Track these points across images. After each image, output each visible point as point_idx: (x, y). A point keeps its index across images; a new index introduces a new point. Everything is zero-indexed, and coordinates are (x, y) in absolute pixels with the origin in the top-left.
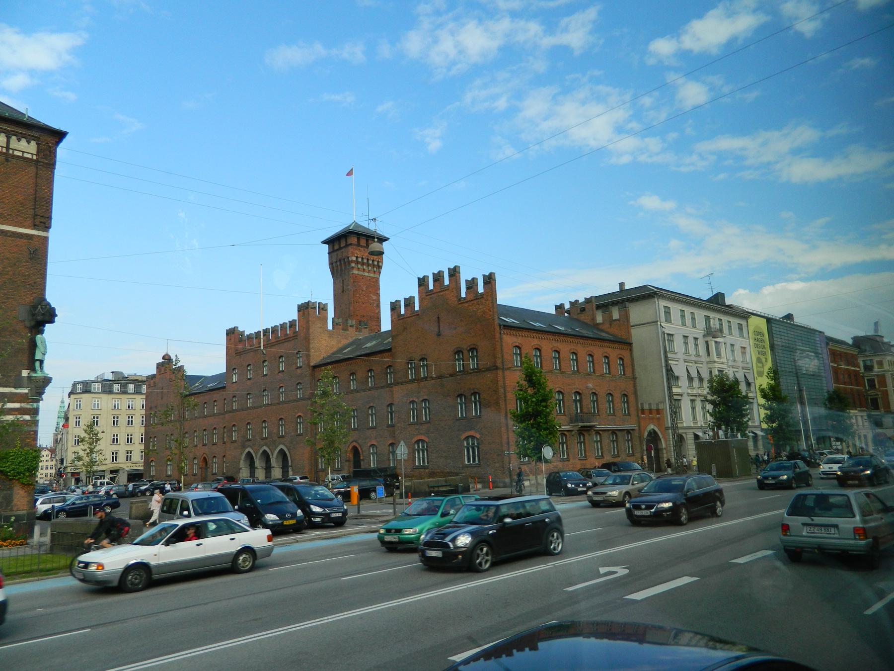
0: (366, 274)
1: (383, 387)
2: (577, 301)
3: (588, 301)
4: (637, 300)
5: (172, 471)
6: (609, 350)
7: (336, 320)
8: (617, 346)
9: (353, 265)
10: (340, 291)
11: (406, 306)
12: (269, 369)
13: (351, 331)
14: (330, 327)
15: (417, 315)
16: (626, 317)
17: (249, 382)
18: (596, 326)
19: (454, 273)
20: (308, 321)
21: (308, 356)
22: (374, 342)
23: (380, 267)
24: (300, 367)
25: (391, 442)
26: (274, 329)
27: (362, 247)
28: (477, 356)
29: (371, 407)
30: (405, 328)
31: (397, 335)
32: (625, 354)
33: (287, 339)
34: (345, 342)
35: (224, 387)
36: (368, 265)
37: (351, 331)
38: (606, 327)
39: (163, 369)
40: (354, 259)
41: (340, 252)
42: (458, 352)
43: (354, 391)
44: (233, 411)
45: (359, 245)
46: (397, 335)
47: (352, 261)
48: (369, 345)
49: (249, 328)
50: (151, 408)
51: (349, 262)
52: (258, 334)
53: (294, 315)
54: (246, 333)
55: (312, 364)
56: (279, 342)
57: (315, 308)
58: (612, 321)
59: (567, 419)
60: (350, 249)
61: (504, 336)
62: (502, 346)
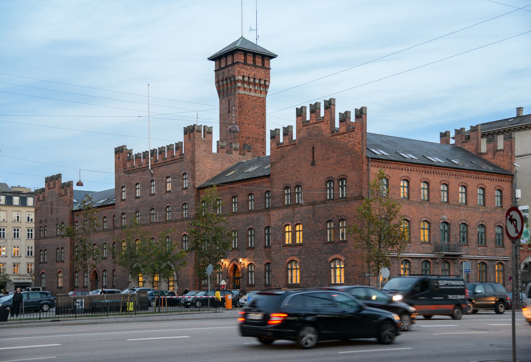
0: (253, 94)
1: (261, 211)
2: (464, 129)
3: (474, 129)
4: (524, 129)
5: (64, 282)
6: (485, 182)
7: (220, 143)
8: (495, 177)
9: (239, 84)
10: (227, 111)
11: (285, 135)
12: (157, 189)
13: (235, 154)
14: (214, 150)
15: (293, 144)
16: (511, 148)
17: (137, 201)
18: (479, 156)
19: (329, 105)
20: (193, 144)
21: (193, 178)
22: (256, 167)
23: (266, 87)
24: (186, 188)
25: (267, 261)
26: (161, 151)
27: (248, 65)
28: (333, 188)
29: (251, 229)
30: (283, 157)
31: (276, 162)
32: (506, 186)
33: (174, 160)
34: (228, 165)
35: (114, 204)
36: (255, 84)
37: (235, 154)
38: (489, 157)
39: (52, 183)
40: (240, 78)
41: (226, 70)
42: (330, 181)
43: (235, 213)
44: (122, 227)
45: (245, 63)
46: (276, 162)
47: (238, 81)
48: (251, 169)
49: (138, 147)
50: (41, 222)
51: (236, 82)
52: (145, 154)
53: (180, 138)
54: (134, 153)
55: (197, 186)
56: (165, 163)
57: (200, 132)
58: (496, 151)
59: (433, 248)
60: (237, 68)
61: (372, 168)
62: (368, 177)
